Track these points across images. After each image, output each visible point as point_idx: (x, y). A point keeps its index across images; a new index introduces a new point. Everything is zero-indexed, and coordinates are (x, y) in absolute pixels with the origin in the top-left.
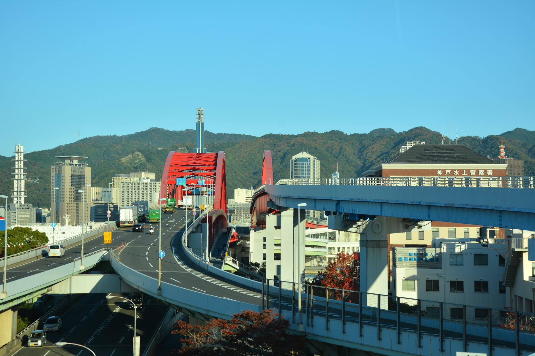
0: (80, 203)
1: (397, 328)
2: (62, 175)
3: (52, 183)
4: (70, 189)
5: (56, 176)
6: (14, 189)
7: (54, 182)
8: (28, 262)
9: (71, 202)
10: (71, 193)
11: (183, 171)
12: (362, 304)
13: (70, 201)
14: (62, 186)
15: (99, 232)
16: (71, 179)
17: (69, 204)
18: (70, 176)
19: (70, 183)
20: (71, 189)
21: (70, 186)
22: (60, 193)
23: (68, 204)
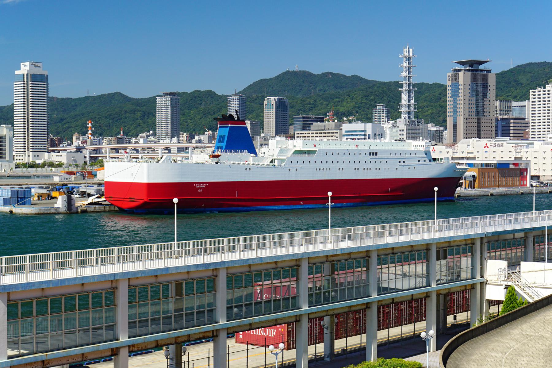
0: (482, 118)
1: (254, 291)
2: (459, 84)
3: (448, 90)
4: (469, 100)
5: (452, 86)
6: (402, 102)
7: (453, 107)
8: (234, 323)
9: (470, 117)
10: (471, 106)
11: (525, 250)
12: (89, 282)
13: (469, 115)
14: (460, 97)
15: (498, 305)
16: (470, 88)
17: (468, 119)
18: (469, 85)
19: (469, 93)
20: (470, 100)
21: (469, 96)
22: (457, 106)
23: (467, 119)
